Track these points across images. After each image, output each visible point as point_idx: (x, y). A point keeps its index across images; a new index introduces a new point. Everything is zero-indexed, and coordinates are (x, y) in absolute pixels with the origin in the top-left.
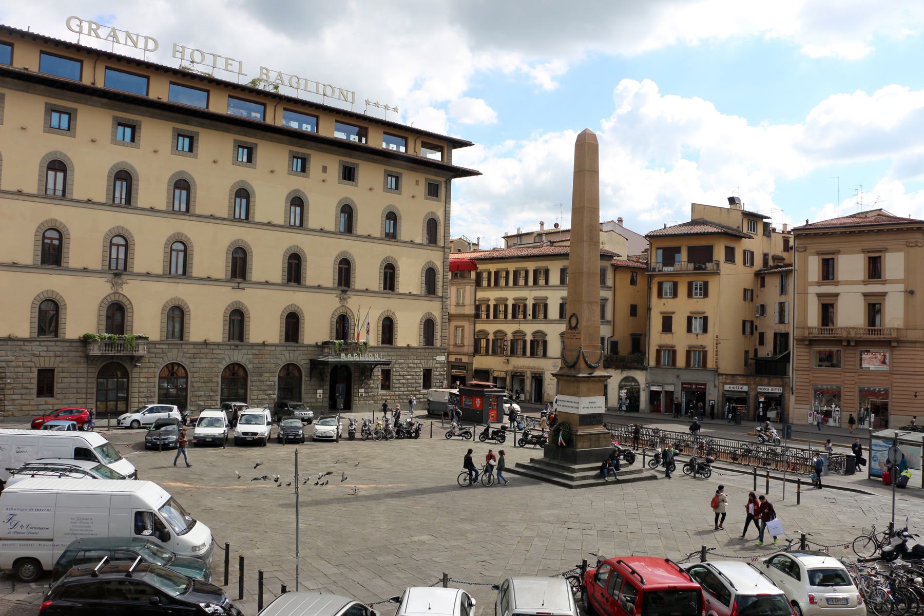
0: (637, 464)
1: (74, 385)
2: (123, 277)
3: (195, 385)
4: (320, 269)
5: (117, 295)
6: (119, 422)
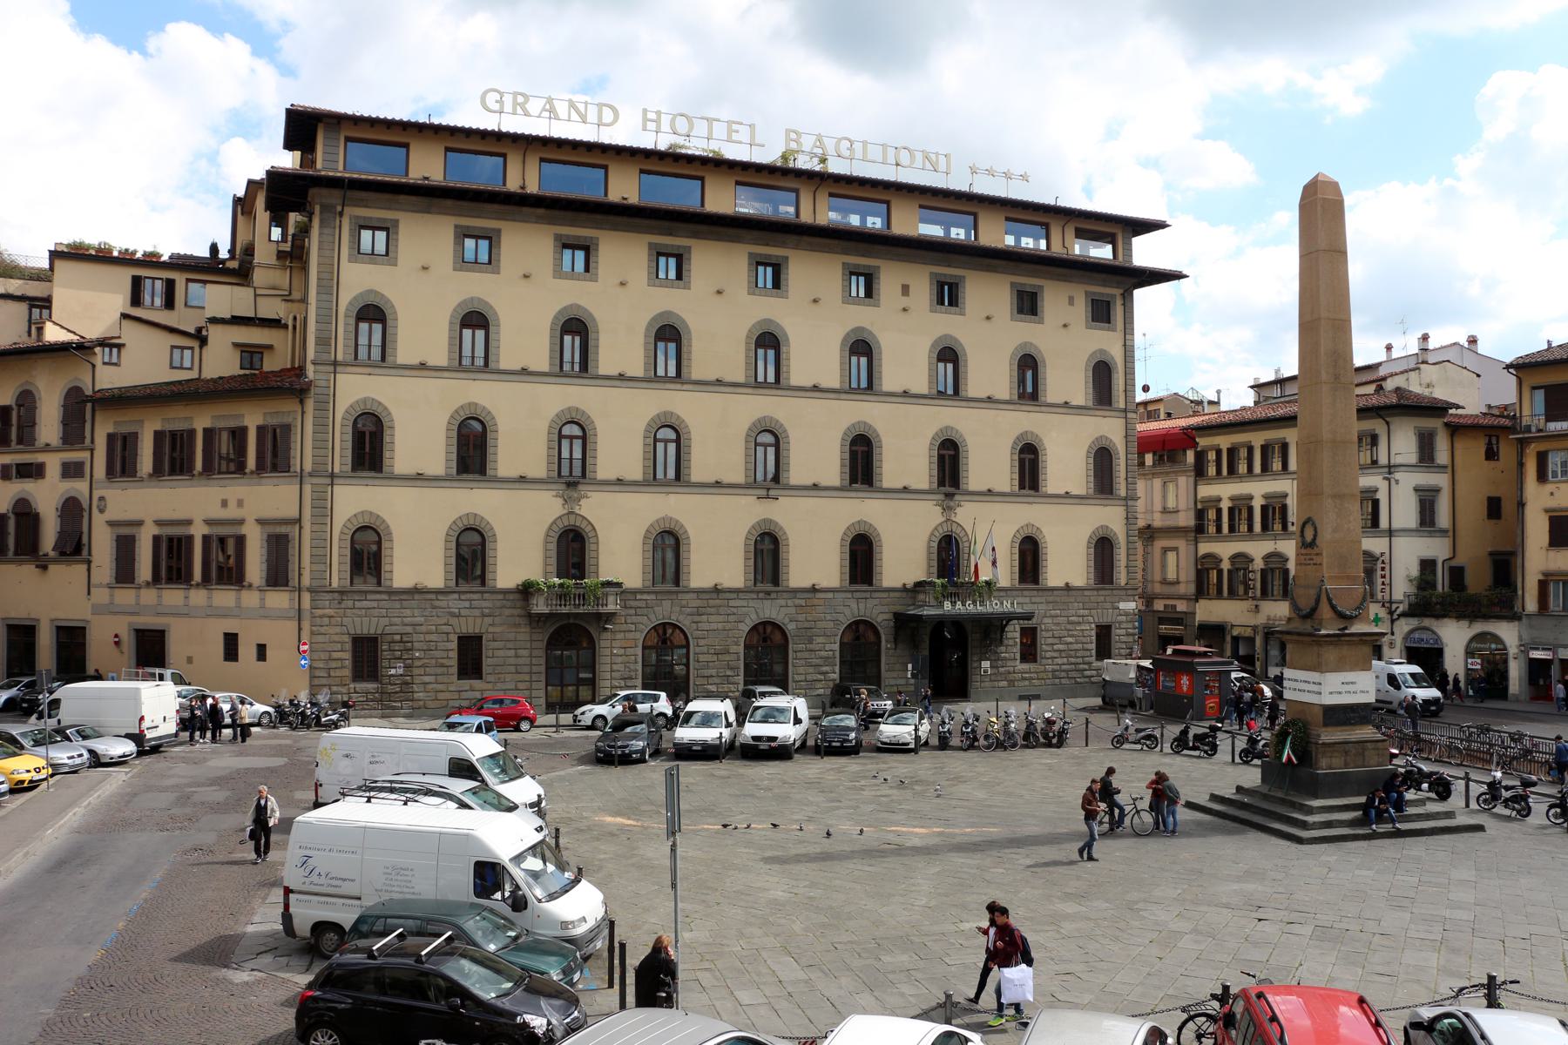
0: (1456, 801)
1: (512, 661)
2: (580, 487)
3: (702, 658)
4: (906, 460)
5: (572, 517)
6: (575, 718)
